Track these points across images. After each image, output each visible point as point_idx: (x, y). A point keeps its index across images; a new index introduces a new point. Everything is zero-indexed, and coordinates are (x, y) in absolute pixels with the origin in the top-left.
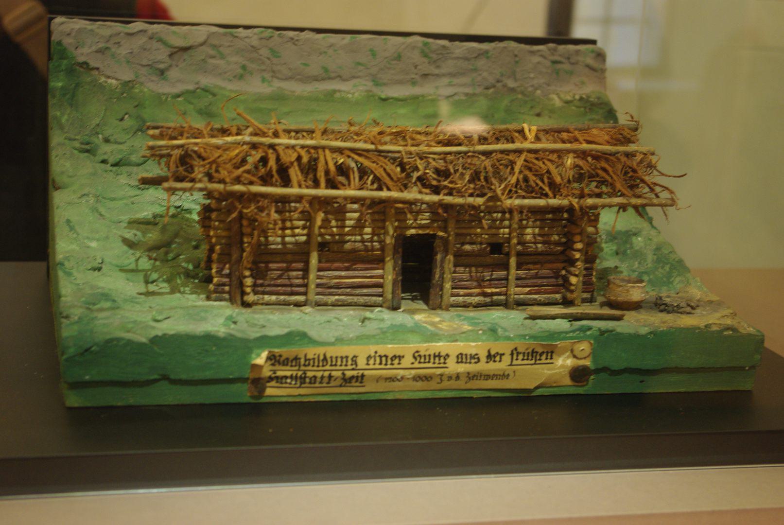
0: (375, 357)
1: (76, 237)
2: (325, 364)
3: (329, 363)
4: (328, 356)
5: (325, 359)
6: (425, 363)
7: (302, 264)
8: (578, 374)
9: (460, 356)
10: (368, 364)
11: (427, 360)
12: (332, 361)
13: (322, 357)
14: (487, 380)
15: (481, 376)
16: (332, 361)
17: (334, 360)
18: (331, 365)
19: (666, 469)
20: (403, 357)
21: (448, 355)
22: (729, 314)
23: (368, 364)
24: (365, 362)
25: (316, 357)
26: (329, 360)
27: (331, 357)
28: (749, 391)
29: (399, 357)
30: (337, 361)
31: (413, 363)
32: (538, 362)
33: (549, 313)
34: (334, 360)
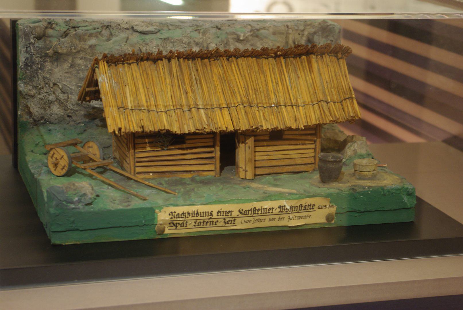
0: (261, 209)
1: (295, 105)
2: (198, 215)
3: (200, 216)
4: (199, 212)
5: (197, 213)
6: (246, 214)
7: (120, 69)
8: (329, 218)
9: (178, 215)
10: (218, 215)
11: (247, 213)
12: (201, 215)
13: (196, 212)
14: (299, 219)
15: (259, 220)
16: (201, 215)
17: (202, 214)
18: (201, 216)
19: (106, 281)
20: (233, 211)
21: (314, 205)
22: (164, 59)
23: (218, 215)
24: (217, 214)
25: (193, 212)
26: (200, 214)
27: (200, 213)
28: (412, 222)
29: (231, 211)
30: (203, 214)
31: (238, 215)
32: (293, 212)
33: (147, 153)
34: (202, 214)
